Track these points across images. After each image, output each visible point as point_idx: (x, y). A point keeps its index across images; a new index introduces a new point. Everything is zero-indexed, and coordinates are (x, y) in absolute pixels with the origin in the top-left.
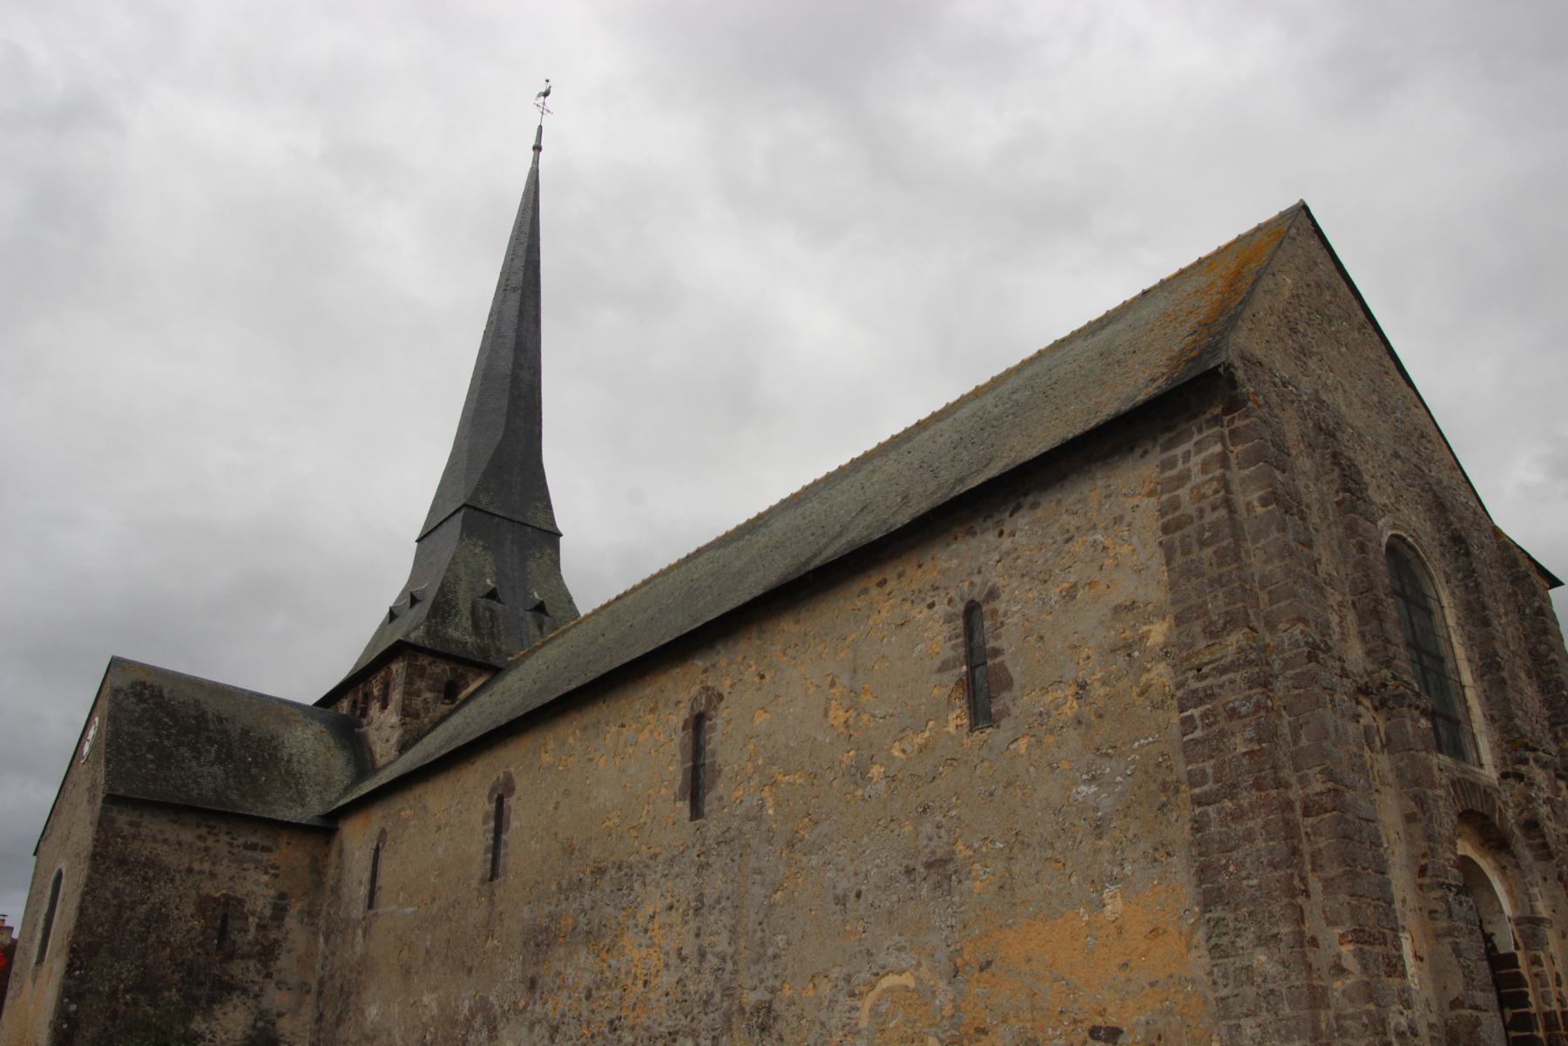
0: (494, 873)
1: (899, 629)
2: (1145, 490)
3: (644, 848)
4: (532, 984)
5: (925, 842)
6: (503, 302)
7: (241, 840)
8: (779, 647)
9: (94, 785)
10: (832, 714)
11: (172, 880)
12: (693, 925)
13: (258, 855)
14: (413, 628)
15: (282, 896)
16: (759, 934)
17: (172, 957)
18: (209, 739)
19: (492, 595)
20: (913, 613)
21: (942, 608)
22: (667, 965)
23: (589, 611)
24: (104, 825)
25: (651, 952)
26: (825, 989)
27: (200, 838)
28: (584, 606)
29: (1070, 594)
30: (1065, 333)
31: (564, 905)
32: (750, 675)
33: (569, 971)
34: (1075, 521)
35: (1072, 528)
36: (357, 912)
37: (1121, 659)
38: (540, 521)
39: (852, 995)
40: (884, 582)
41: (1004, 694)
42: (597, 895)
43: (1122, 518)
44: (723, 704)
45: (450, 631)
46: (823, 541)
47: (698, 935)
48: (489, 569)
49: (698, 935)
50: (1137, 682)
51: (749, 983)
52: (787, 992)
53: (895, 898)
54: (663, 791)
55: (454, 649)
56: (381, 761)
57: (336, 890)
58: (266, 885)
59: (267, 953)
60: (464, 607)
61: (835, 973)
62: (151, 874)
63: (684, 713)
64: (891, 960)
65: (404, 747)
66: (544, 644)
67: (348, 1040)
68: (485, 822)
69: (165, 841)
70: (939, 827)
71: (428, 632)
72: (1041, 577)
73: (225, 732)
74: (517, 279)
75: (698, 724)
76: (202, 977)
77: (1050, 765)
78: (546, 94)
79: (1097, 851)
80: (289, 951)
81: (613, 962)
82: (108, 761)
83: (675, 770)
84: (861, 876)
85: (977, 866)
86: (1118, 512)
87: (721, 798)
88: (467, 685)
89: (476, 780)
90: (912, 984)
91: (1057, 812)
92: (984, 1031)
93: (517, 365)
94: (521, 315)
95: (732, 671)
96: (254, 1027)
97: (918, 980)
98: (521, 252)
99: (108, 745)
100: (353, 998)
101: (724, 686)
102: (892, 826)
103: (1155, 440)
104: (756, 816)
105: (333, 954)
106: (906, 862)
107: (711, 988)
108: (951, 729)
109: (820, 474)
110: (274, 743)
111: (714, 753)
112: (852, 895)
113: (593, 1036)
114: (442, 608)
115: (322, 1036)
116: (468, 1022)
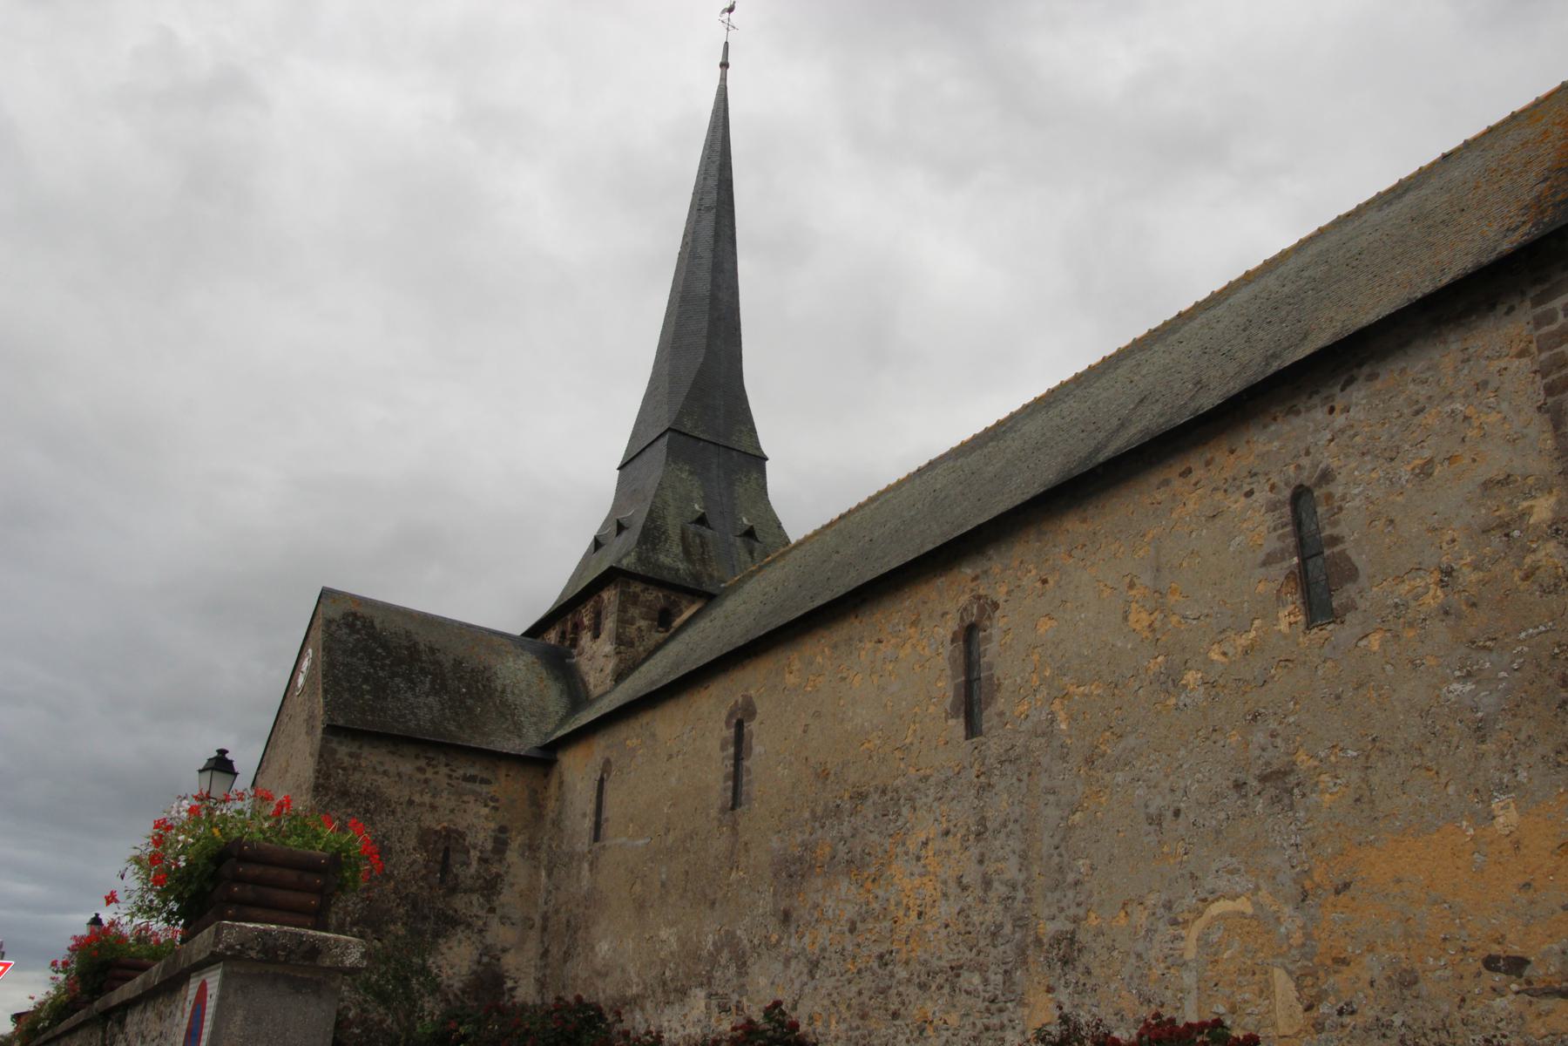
0: (736, 802)
1: (1219, 519)
2: (1514, 351)
3: (912, 771)
4: (786, 917)
5: (1258, 752)
6: (698, 222)
7: (461, 772)
8: (1063, 548)
9: (311, 717)
10: (1132, 618)
11: (393, 812)
12: (974, 851)
13: (477, 787)
14: (622, 552)
15: (503, 829)
16: (1056, 859)
17: (396, 891)
18: (422, 670)
19: (702, 520)
20: (1227, 503)
21: (1262, 496)
22: (945, 895)
23: (801, 537)
24: (324, 757)
25: (925, 882)
26: (1141, 917)
27: (420, 769)
28: (795, 533)
29: (1425, 471)
30: (1350, 206)
31: (820, 832)
32: (1030, 580)
33: (829, 903)
34: (1424, 391)
35: (1422, 400)
36: (583, 844)
37: (1496, 540)
38: (745, 445)
39: (1174, 922)
40: (1189, 471)
41: (1348, 586)
42: (858, 821)
43: (1485, 383)
44: (998, 613)
45: (662, 557)
46: (1101, 436)
47: (981, 862)
48: (697, 493)
49: (981, 862)
50: (1519, 566)
51: (1046, 912)
52: (1093, 921)
53: (1222, 815)
54: (932, 709)
55: (666, 576)
56: (595, 692)
57: (557, 823)
58: (486, 818)
59: (490, 887)
60: (674, 533)
61: (1151, 900)
62: (372, 806)
63: (952, 624)
64: (1222, 884)
65: (619, 677)
66: (760, 569)
67: (577, 976)
68: (723, 748)
69: (385, 773)
70: (1273, 735)
71: (639, 559)
72: (1386, 455)
73: (438, 663)
74: (711, 199)
75: (969, 635)
76: (426, 911)
77: (1412, 662)
78: (731, 10)
79: (1480, 757)
80: (512, 885)
81: (881, 893)
82: (326, 691)
83: (945, 686)
84: (1179, 793)
85: (1324, 777)
86: (1480, 378)
87: (1001, 714)
88: (681, 612)
89: (709, 708)
90: (1249, 910)
91: (1424, 714)
92: (1345, 962)
93: (715, 285)
94: (717, 236)
95: (1007, 576)
96: (479, 962)
97: (1257, 905)
98: (714, 170)
99: (325, 676)
100: (580, 933)
101: (1000, 594)
102: (1214, 736)
103: (1523, 293)
104: (1047, 731)
105: (558, 888)
106: (1234, 776)
107: (999, 919)
108: (1283, 626)
109: (1016, 407)
110: (487, 674)
111: (990, 666)
112: (1169, 814)
113: (859, 972)
114: (651, 535)
115: (548, 971)
116: (713, 959)
